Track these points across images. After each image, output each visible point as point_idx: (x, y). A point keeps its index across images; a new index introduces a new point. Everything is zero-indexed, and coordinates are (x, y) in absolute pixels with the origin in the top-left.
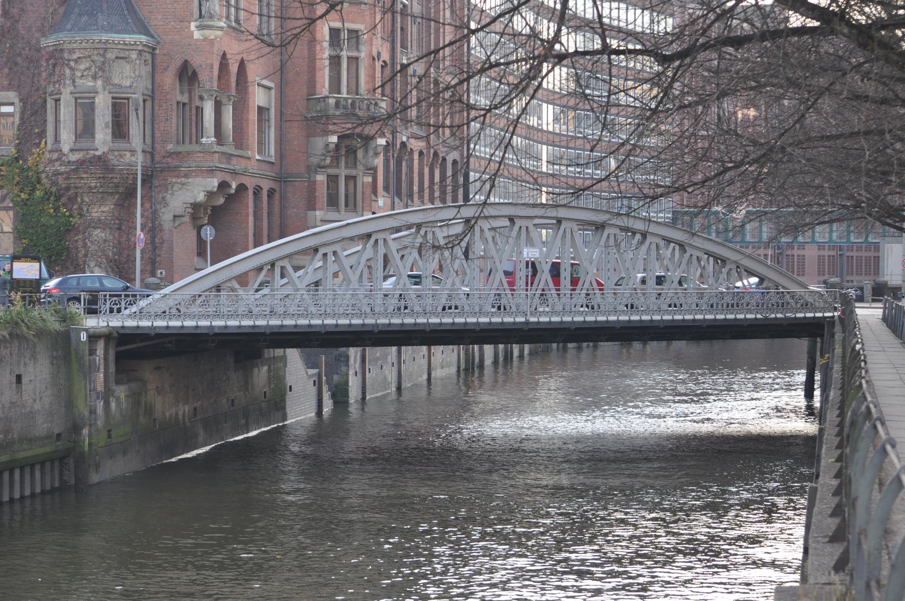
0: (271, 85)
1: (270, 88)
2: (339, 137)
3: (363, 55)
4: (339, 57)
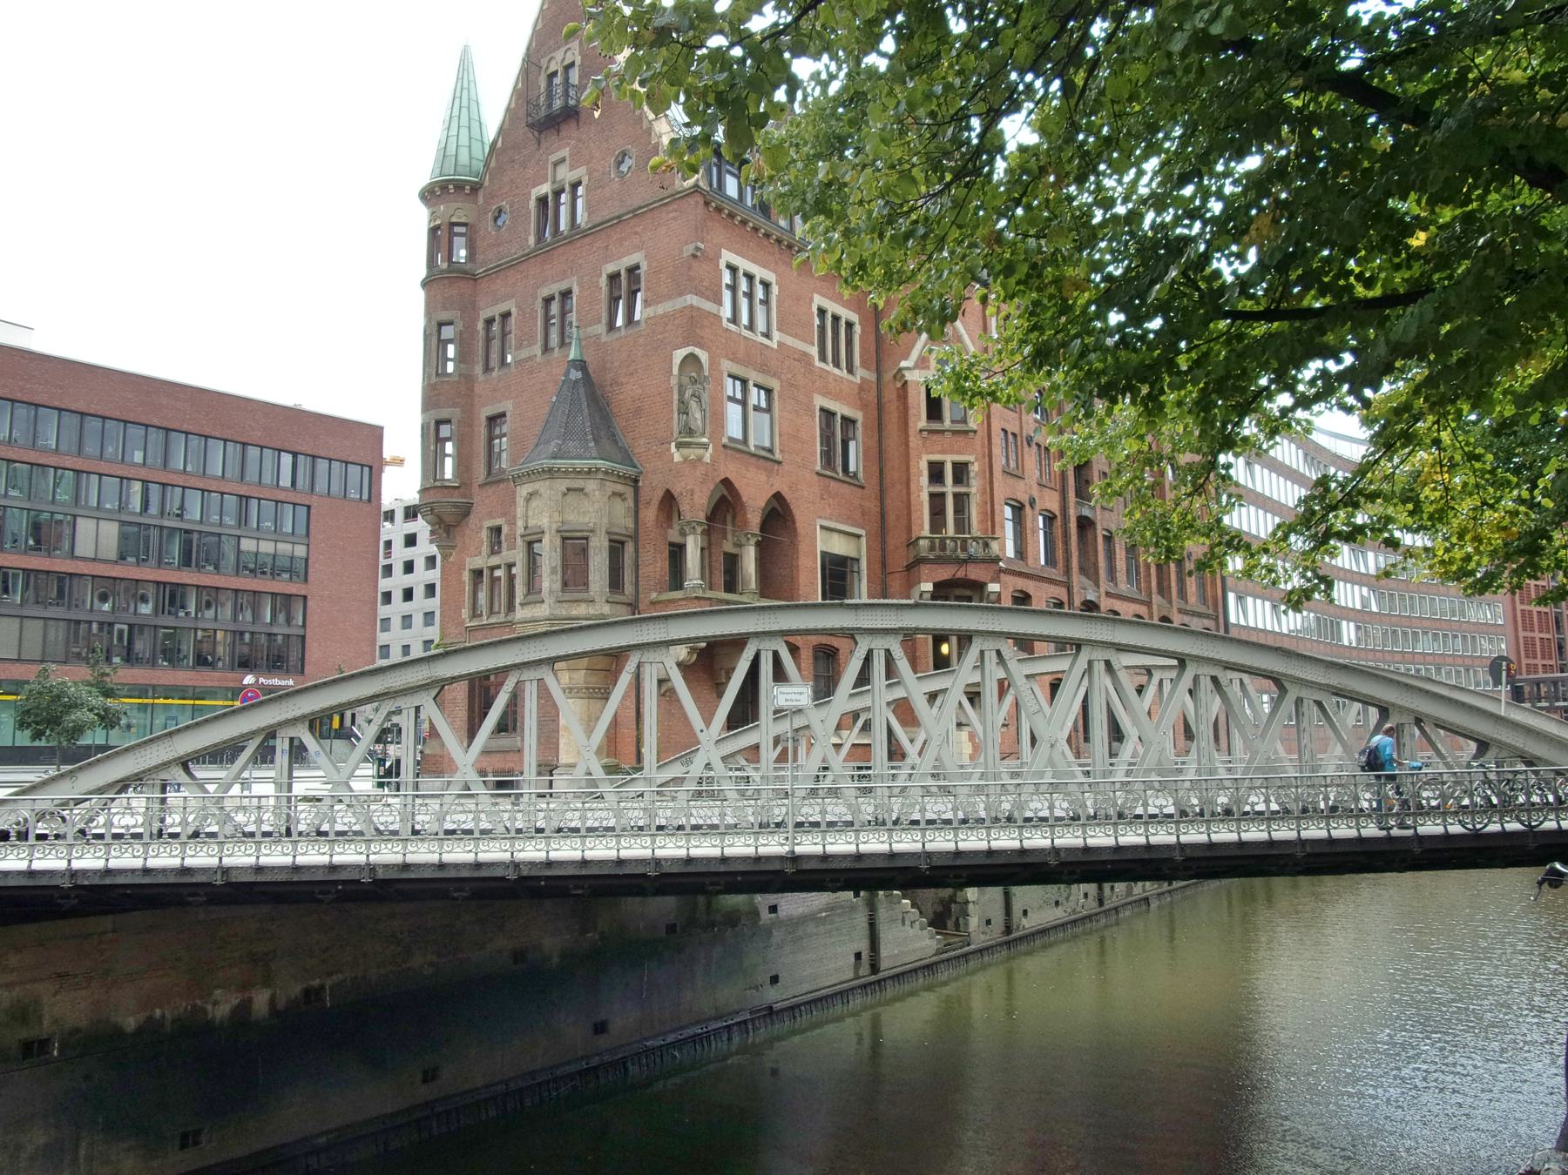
0: (862, 532)
1: (859, 536)
2: (935, 585)
3: (973, 490)
4: (943, 495)
